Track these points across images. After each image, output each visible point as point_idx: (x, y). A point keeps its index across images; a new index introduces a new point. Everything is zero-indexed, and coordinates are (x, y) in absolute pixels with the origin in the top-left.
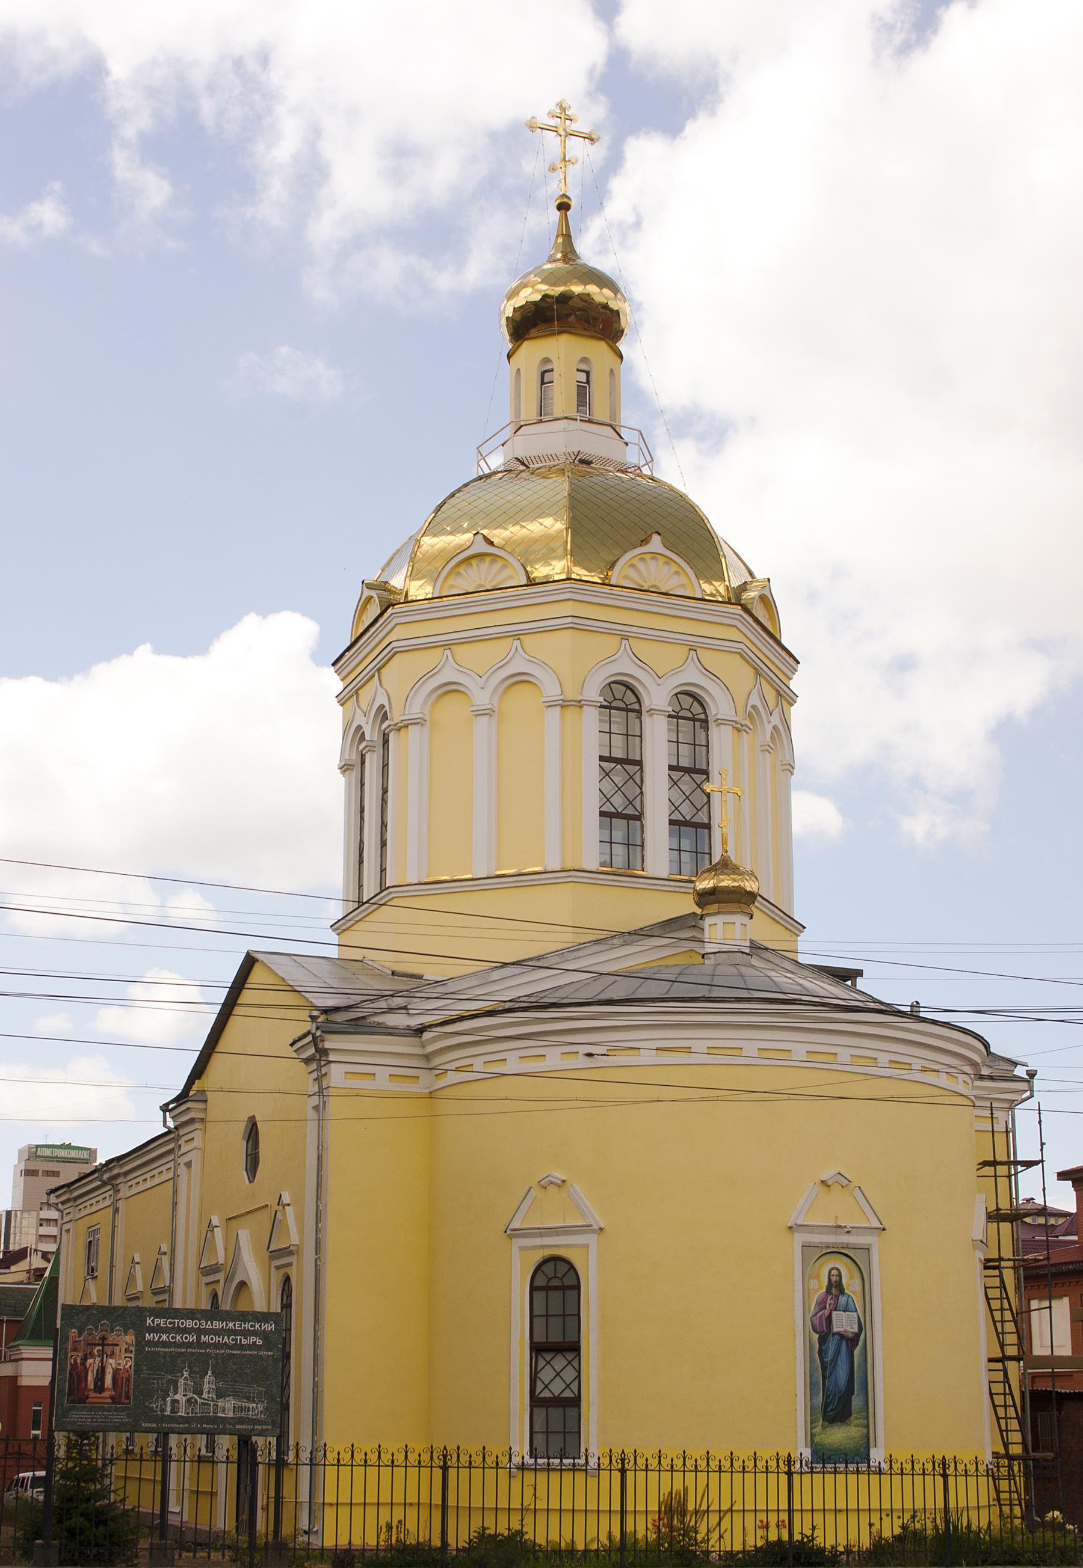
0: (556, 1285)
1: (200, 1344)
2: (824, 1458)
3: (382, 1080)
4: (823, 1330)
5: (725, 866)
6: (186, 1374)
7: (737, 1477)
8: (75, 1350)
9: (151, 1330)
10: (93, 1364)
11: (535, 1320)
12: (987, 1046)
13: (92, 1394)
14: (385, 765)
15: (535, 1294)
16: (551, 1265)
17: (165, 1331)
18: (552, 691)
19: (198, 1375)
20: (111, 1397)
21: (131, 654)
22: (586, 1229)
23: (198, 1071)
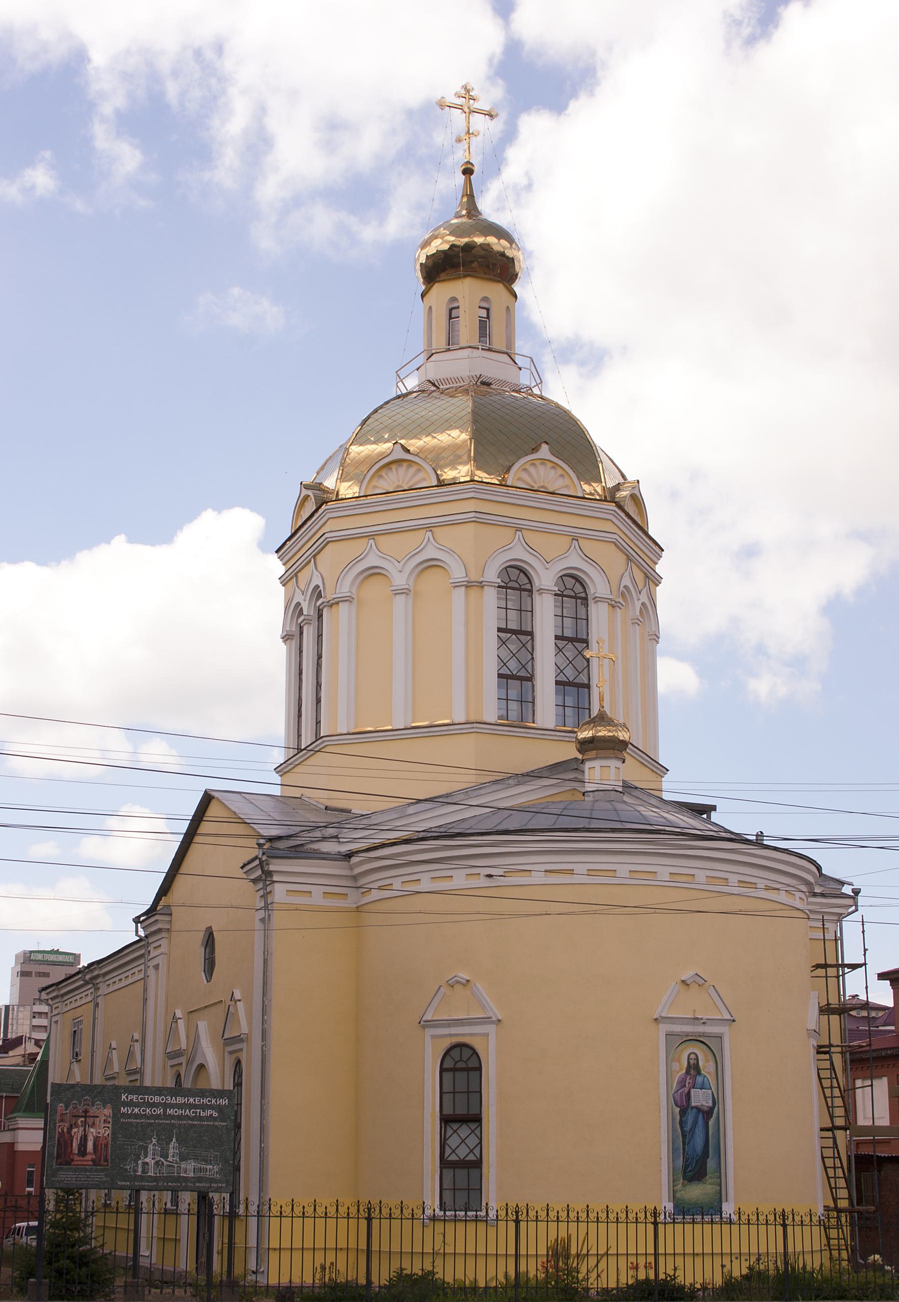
0: (462, 1066)
1: (166, 1116)
2: (684, 1211)
3: (317, 897)
4: (683, 1104)
5: (602, 719)
6: (154, 1141)
7: (612, 1226)
8: (62, 1121)
9: (125, 1104)
10: (77, 1132)
11: (444, 1096)
12: (819, 868)
13: (76, 1158)
14: (320, 635)
15: (444, 1074)
16: (458, 1050)
17: (137, 1105)
18: (458, 573)
19: (164, 1142)
20: (92, 1160)
21: (109, 543)
22: (486, 1020)
23: (165, 890)
